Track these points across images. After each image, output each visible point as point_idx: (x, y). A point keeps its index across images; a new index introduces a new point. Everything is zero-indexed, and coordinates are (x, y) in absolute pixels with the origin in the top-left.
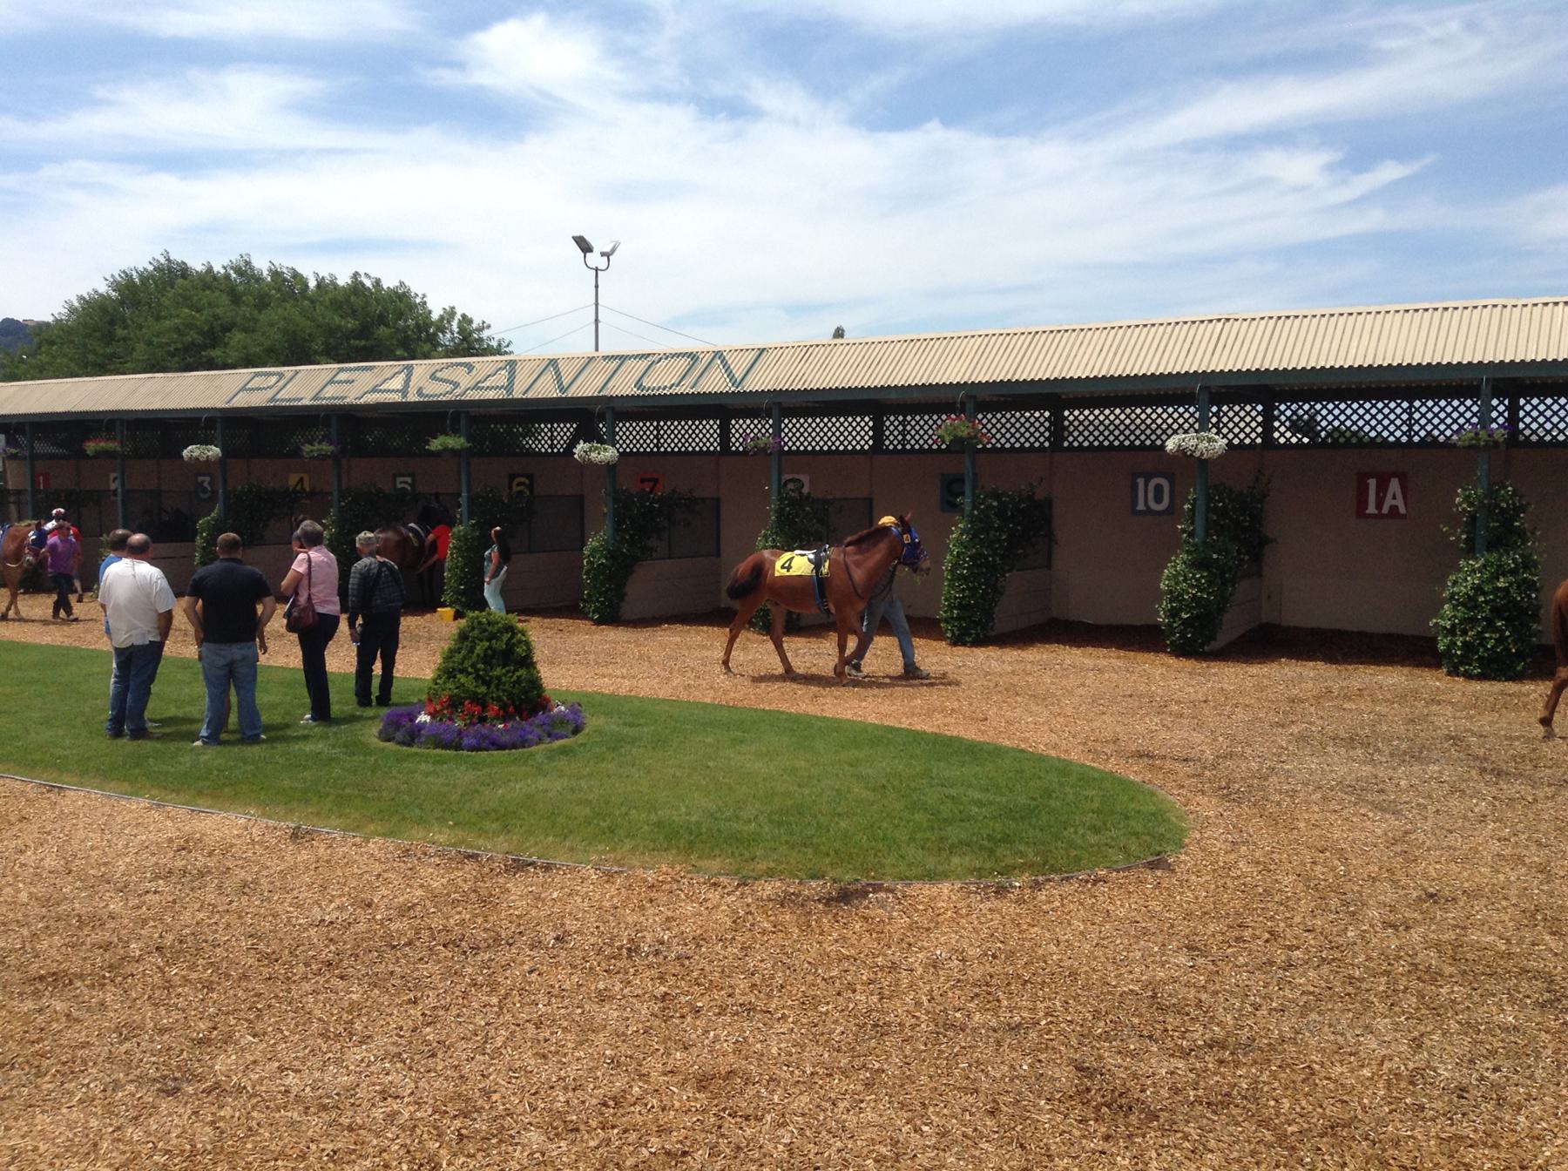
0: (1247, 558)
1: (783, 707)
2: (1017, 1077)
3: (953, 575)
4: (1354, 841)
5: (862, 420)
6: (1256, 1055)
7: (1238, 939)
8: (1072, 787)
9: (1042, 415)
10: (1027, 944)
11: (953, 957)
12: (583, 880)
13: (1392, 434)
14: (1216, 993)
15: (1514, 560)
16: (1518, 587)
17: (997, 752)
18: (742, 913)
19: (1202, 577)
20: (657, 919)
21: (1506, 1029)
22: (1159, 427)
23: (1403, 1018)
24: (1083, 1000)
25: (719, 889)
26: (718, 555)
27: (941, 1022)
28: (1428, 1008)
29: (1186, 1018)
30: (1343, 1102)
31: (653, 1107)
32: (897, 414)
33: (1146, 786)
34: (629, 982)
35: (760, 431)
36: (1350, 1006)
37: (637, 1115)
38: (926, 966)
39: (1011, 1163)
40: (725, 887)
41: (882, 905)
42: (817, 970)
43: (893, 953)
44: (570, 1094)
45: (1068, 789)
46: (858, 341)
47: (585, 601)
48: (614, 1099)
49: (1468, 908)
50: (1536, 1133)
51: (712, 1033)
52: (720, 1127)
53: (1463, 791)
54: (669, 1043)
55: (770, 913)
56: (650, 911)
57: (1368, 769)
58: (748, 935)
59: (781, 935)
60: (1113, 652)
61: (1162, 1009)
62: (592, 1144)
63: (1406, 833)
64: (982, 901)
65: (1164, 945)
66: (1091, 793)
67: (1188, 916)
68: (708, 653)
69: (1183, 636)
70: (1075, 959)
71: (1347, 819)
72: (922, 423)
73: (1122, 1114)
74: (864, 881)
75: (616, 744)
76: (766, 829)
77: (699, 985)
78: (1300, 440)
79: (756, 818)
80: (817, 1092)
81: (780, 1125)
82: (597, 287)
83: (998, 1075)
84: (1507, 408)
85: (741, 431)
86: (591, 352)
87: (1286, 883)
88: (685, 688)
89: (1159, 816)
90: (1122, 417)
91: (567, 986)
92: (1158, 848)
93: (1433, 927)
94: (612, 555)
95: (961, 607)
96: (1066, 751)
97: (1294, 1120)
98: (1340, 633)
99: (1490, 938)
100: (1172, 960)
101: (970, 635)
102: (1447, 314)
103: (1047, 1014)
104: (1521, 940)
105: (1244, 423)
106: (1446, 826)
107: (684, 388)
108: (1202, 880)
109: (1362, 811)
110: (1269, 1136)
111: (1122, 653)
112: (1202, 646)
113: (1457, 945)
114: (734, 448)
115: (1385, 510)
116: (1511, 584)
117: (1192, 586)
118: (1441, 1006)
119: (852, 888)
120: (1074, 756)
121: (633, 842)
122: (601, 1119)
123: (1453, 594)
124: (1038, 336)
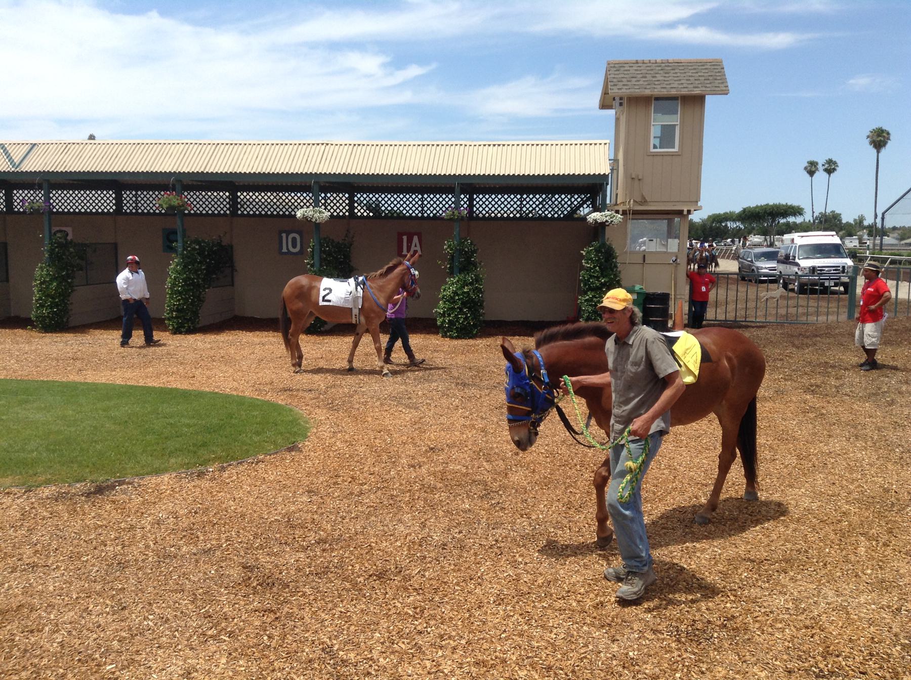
1: (57, 378)
2: (208, 578)
5: (74, 193)
6: (342, 544)
7: (335, 484)
8: (245, 411)
9: (224, 194)
10: (216, 503)
11: (170, 517)
13: (408, 212)
15: (472, 277)
17: (200, 395)
18: (27, 508)
21: (465, 512)
24: (248, 529)
25: (12, 496)
26: (7, 280)
27: (161, 555)
28: (429, 506)
29: (306, 530)
32: (131, 189)
33: (288, 406)
38: (153, 524)
40: (15, 494)
41: (124, 492)
42: (80, 536)
45: (242, 412)
50: (478, 560)
51: (7, 585)
55: (48, 506)
57: (403, 387)
58: (33, 521)
59: (56, 519)
60: (271, 333)
61: (293, 527)
63: (421, 418)
64: (189, 482)
66: (256, 413)
70: (244, 507)
72: (79, 195)
73: (268, 588)
74: (113, 480)
78: (368, 214)
79: (36, 450)
81: (54, 632)
83: (196, 579)
89: (295, 422)
90: (272, 197)
93: (433, 465)
95: (178, 310)
96: (242, 391)
97: (361, 575)
99: (458, 467)
100: (299, 499)
101: (184, 327)
102: (439, 148)
103: (227, 540)
104: (473, 466)
105: (338, 204)
108: (316, 455)
109: (400, 409)
110: (348, 585)
112: (320, 328)
113: (443, 472)
114: (16, 210)
116: (470, 290)
119: (104, 485)
120: (247, 394)
123: (444, 296)
124: (218, 146)
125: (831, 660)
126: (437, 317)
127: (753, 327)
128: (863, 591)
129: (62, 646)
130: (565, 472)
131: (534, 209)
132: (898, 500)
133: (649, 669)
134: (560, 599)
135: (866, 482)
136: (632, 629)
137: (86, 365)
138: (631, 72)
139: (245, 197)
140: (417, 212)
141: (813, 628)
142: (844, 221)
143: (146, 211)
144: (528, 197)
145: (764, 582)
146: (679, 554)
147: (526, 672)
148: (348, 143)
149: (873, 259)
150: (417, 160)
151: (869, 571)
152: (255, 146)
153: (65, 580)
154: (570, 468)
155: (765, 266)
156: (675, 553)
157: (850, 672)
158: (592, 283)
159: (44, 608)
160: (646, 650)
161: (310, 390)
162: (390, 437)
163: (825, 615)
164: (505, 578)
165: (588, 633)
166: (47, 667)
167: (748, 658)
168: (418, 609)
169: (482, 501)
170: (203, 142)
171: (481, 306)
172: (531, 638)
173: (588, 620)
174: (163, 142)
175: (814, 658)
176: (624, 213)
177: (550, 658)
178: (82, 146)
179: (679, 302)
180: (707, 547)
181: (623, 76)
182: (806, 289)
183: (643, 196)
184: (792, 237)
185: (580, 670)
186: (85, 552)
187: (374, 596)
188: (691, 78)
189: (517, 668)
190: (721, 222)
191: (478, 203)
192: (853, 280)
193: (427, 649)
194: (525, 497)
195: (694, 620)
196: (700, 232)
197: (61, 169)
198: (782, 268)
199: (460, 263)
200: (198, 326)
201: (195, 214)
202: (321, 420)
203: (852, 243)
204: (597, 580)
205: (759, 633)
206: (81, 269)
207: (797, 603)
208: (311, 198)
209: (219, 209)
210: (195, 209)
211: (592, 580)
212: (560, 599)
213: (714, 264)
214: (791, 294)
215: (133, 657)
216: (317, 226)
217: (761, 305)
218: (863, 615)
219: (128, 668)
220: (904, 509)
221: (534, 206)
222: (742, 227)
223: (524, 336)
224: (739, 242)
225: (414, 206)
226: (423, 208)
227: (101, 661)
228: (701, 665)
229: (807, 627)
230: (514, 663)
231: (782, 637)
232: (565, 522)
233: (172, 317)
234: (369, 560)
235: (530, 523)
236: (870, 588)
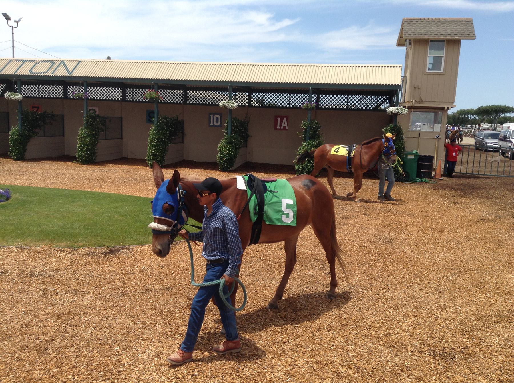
1: (89, 190)
2: (169, 303)
3: (151, 145)
5: (100, 88)
9: (180, 92)
10: (173, 262)
12: (12, 252)
13: (298, 104)
15: (316, 143)
18: (73, 260)
19: (230, 147)
20: (41, 264)
21: (310, 276)
22: (217, 98)
26: (63, 135)
30: (266, 301)
31: (40, 326)
34: (31, 286)
35: (79, 91)
37: (35, 329)
38: (139, 272)
39: (166, 330)
40: (67, 251)
41: (125, 253)
43: (129, 269)
44: (8, 325)
46: (115, 61)
47: (10, 152)
48: (26, 325)
49: (301, 243)
51: (63, 300)
52: (66, 330)
54: (46, 305)
56: (39, 261)
60: (203, 170)
62: (17, 341)
68: (60, 171)
69: (224, 165)
74: (119, 246)
75: (23, 204)
76: (83, 231)
77: (57, 284)
79: (79, 227)
80: (101, 316)
82: (13, 33)
83: (163, 303)
84: (316, 98)
85: (72, 91)
86: (12, 58)
88: (51, 184)
91: (6, 288)
94: (21, 135)
95: (154, 156)
98: (206, 162)
99: (307, 251)
103: (179, 283)
105: (242, 98)
107: (49, 73)
111: (205, 171)
112: (229, 168)
114: (69, 97)
115: (282, 127)
117: (227, 150)
121: (31, 238)
122: (20, 332)
123: (300, 153)
126: (295, 164)
127: (483, 178)
129: (91, 335)
131: (355, 104)
133: (416, 373)
134: (365, 329)
136: (407, 349)
137: (105, 183)
138: (417, 25)
139: (191, 94)
140: (286, 104)
143: (138, 100)
144: (352, 96)
145: (486, 328)
146: (436, 309)
147: (345, 370)
148: (250, 64)
150: (288, 75)
152: (198, 65)
153: (93, 300)
154: (372, 255)
155: (491, 142)
156: (434, 308)
159: (82, 314)
160: (415, 362)
164: (333, 316)
165: (382, 350)
166: (84, 346)
168: (284, 329)
169: (320, 271)
170: (170, 62)
172: (348, 350)
173: (381, 343)
174: (148, 62)
176: (409, 108)
177: (359, 363)
178: (105, 63)
179: (439, 161)
181: (412, 27)
183: (420, 98)
184: (508, 125)
185: (376, 371)
186: (104, 285)
188: (453, 29)
189: (340, 367)
190: (465, 115)
191: (322, 99)
193: (289, 352)
195: (444, 347)
196: (451, 120)
197: (94, 75)
198: (501, 143)
199: (310, 134)
200: (164, 164)
201: (164, 103)
204: (387, 321)
205: (483, 357)
206: (103, 131)
207: (506, 342)
209: (174, 100)
210: (164, 100)
211: (384, 320)
212: (365, 329)
213: (460, 140)
214: (507, 159)
215: (128, 344)
216: (230, 111)
217: (489, 165)
219: (126, 350)
221: (355, 102)
222: (477, 118)
223: (345, 177)
224: (475, 127)
225: (285, 100)
226: (290, 102)
227: (112, 345)
228: (448, 373)
230: (338, 363)
232: (368, 286)
233: (151, 159)
234: (256, 299)
235: (348, 285)
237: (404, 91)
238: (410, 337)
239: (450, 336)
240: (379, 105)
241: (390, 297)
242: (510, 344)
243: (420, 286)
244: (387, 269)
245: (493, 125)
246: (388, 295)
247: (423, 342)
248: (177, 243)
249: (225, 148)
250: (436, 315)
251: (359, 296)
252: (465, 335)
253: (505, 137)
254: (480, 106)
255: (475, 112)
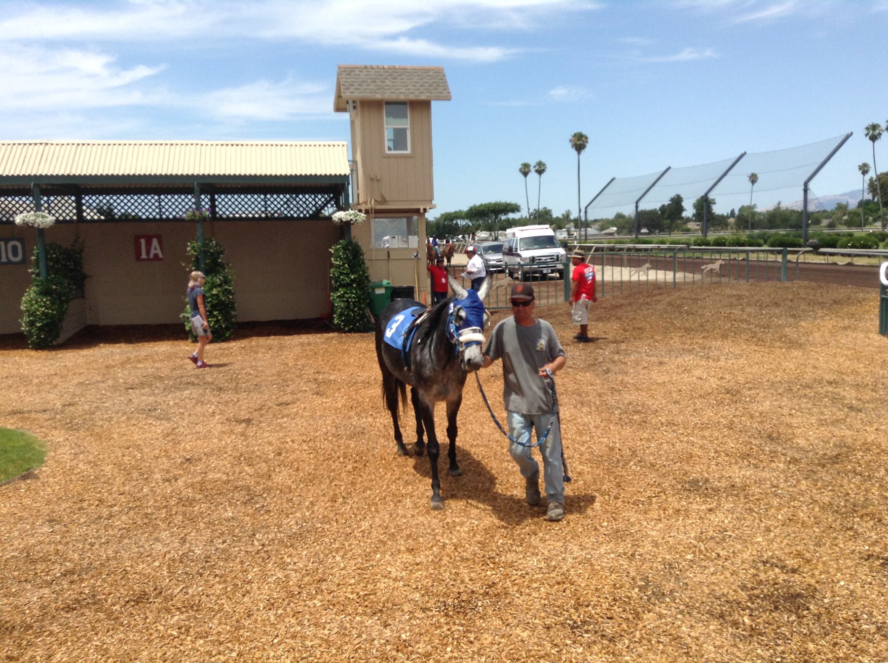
0: (74, 287)
4: (145, 439)
7: (79, 509)
13: (133, 211)
14: (67, 543)
15: (220, 279)
16: (223, 293)
19: (47, 300)
23: (175, 529)
28: (188, 520)
29: (49, 563)
36: (147, 530)
50: (244, 569)
53: (202, 402)
57: (152, 398)
63: (174, 429)
65: (33, 523)
67: (49, 502)
69: (38, 337)
71: (141, 428)
73: (8, 633)
84: (210, 200)
87: (107, 470)
89: (28, 446)
92: (28, 466)
99: (219, 475)
100: (39, 531)
106: (195, 422)
108: (56, 480)
109: (150, 422)
112: (51, 342)
113: (202, 483)
115: (151, 256)
116: (219, 292)
117: (42, 307)
118: (195, 517)
125: (582, 610)
128: (602, 543)
130: (329, 466)
132: (622, 456)
133: (421, 648)
135: (594, 443)
136: (402, 611)
141: (564, 583)
142: (454, 254)
145: (518, 546)
146: (441, 531)
149: (581, 248)
151: (605, 524)
156: (437, 531)
157: (600, 619)
158: (343, 280)
160: (417, 630)
161: (44, 411)
162: (140, 453)
163: (573, 570)
167: (510, 621)
169: (245, 507)
171: (233, 308)
172: (304, 638)
173: (360, 610)
175: (568, 611)
179: (423, 294)
180: (465, 520)
182: (529, 277)
183: (382, 195)
187: (133, 623)
188: (417, 84)
190: (452, 220)
192: (567, 266)
194: (290, 496)
195: (459, 593)
196: (434, 229)
198: (507, 259)
202: (59, 442)
203: (562, 235)
205: (518, 595)
207: (549, 562)
208: (31, 202)
218: (604, 564)
220: (627, 464)
222: (470, 224)
226: (160, 209)
228: (469, 635)
229: (559, 583)
231: (538, 596)
232: (331, 515)
236: (607, 539)
237: (355, 183)
238: (406, 588)
239: (466, 571)
240: (318, 211)
241: (369, 528)
242: (553, 564)
243: (413, 498)
244: (360, 479)
245: (493, 233)
246: (365, 525)
247: (427, 592)
248: (479, 497)
249: (37, 303)
250: (442, 541)
251: (316, 536)
252: (488, 565)
253: (510, 249)
254: (472, 205)
255: (465, 215)
